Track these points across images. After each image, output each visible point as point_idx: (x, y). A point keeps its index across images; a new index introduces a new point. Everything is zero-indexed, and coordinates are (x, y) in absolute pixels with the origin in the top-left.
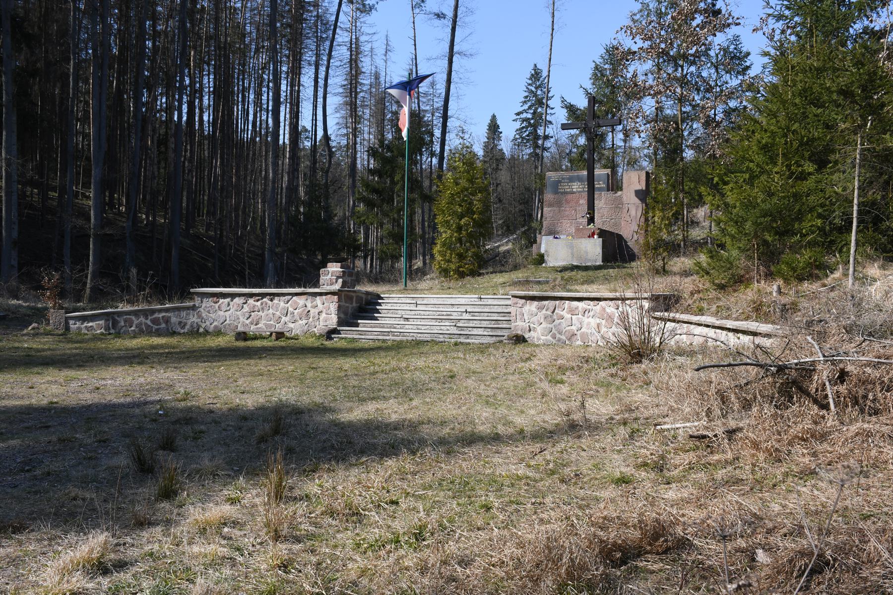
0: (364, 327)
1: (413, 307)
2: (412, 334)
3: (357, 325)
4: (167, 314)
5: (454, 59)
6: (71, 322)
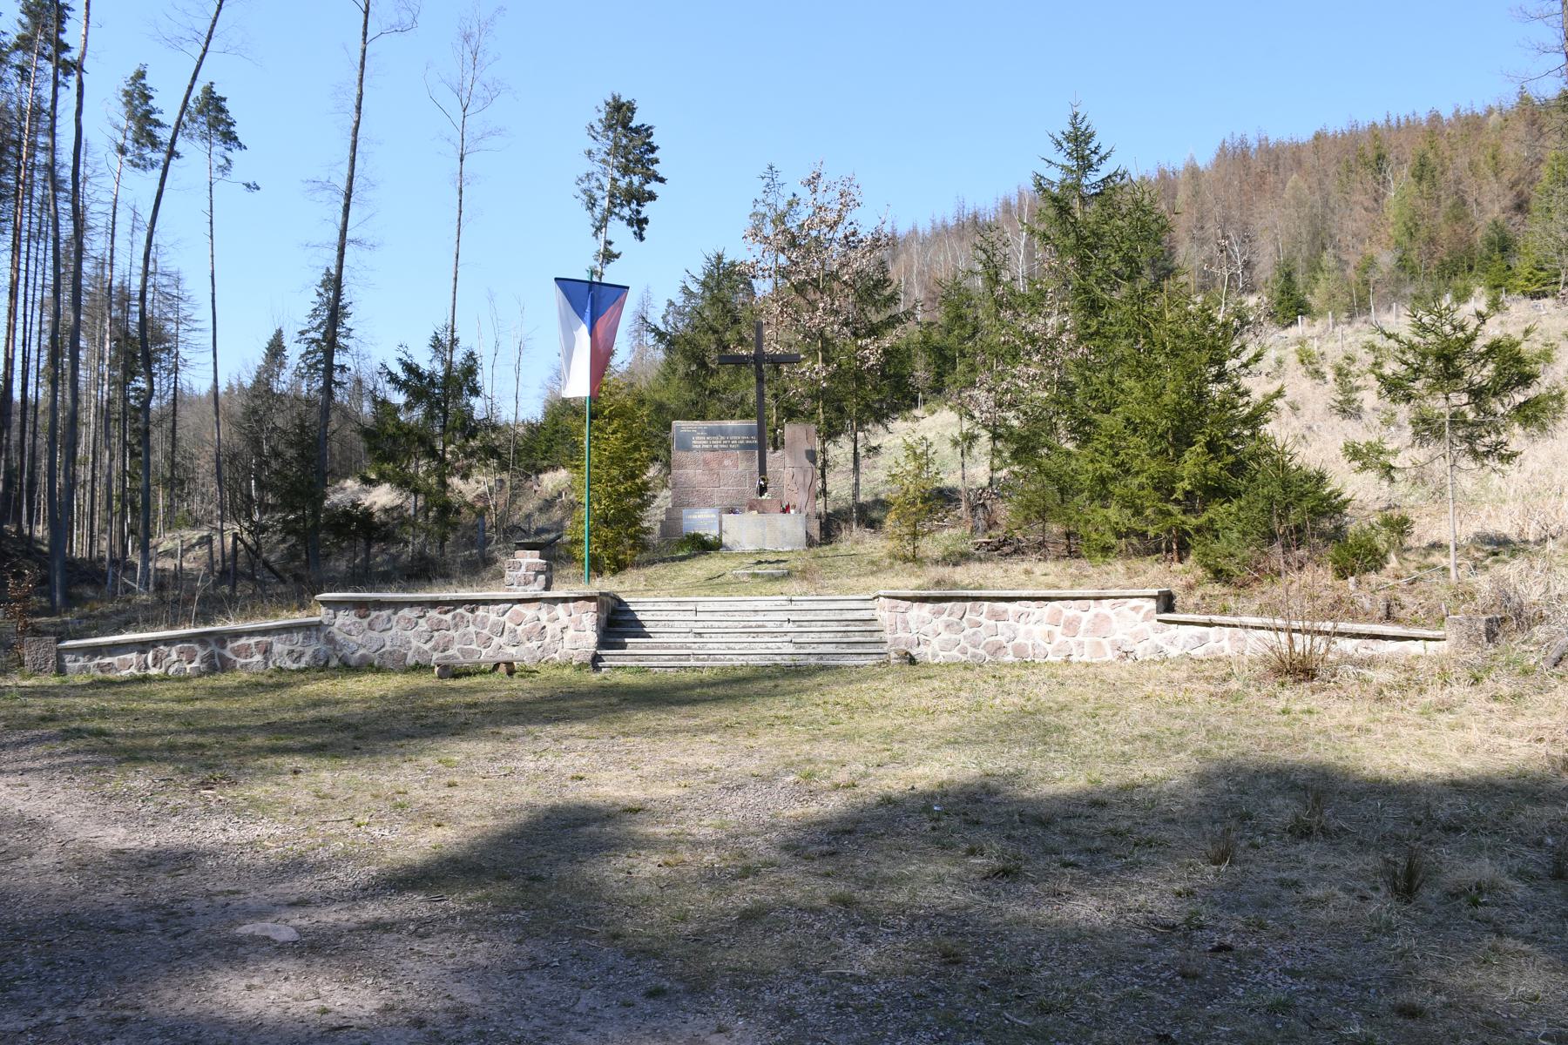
0: (635, 648)
1: (691, 616)
3: (624, 646)
4: (265, 639)
5: (347, 249)
6: (68, 658)
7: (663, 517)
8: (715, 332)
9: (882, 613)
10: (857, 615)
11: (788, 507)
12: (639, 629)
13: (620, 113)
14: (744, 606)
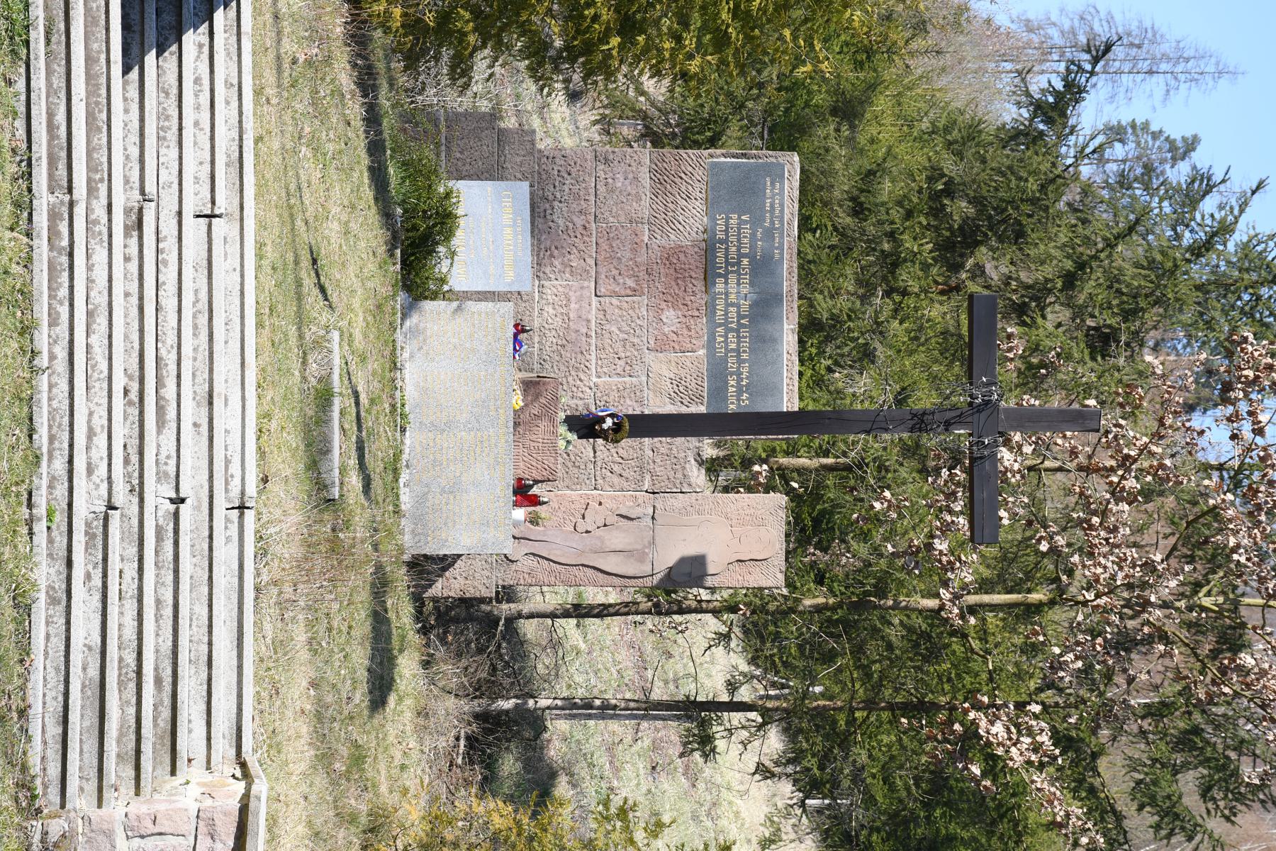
1: (195, 200)
2: (64, 311)
7: (510, 123)
8: (1070, 280)
9: (194, 791)
10: (191, 710)
11: (535, 501)
12: (151, 35)
13: (100, 806)
14: (226, 366)
